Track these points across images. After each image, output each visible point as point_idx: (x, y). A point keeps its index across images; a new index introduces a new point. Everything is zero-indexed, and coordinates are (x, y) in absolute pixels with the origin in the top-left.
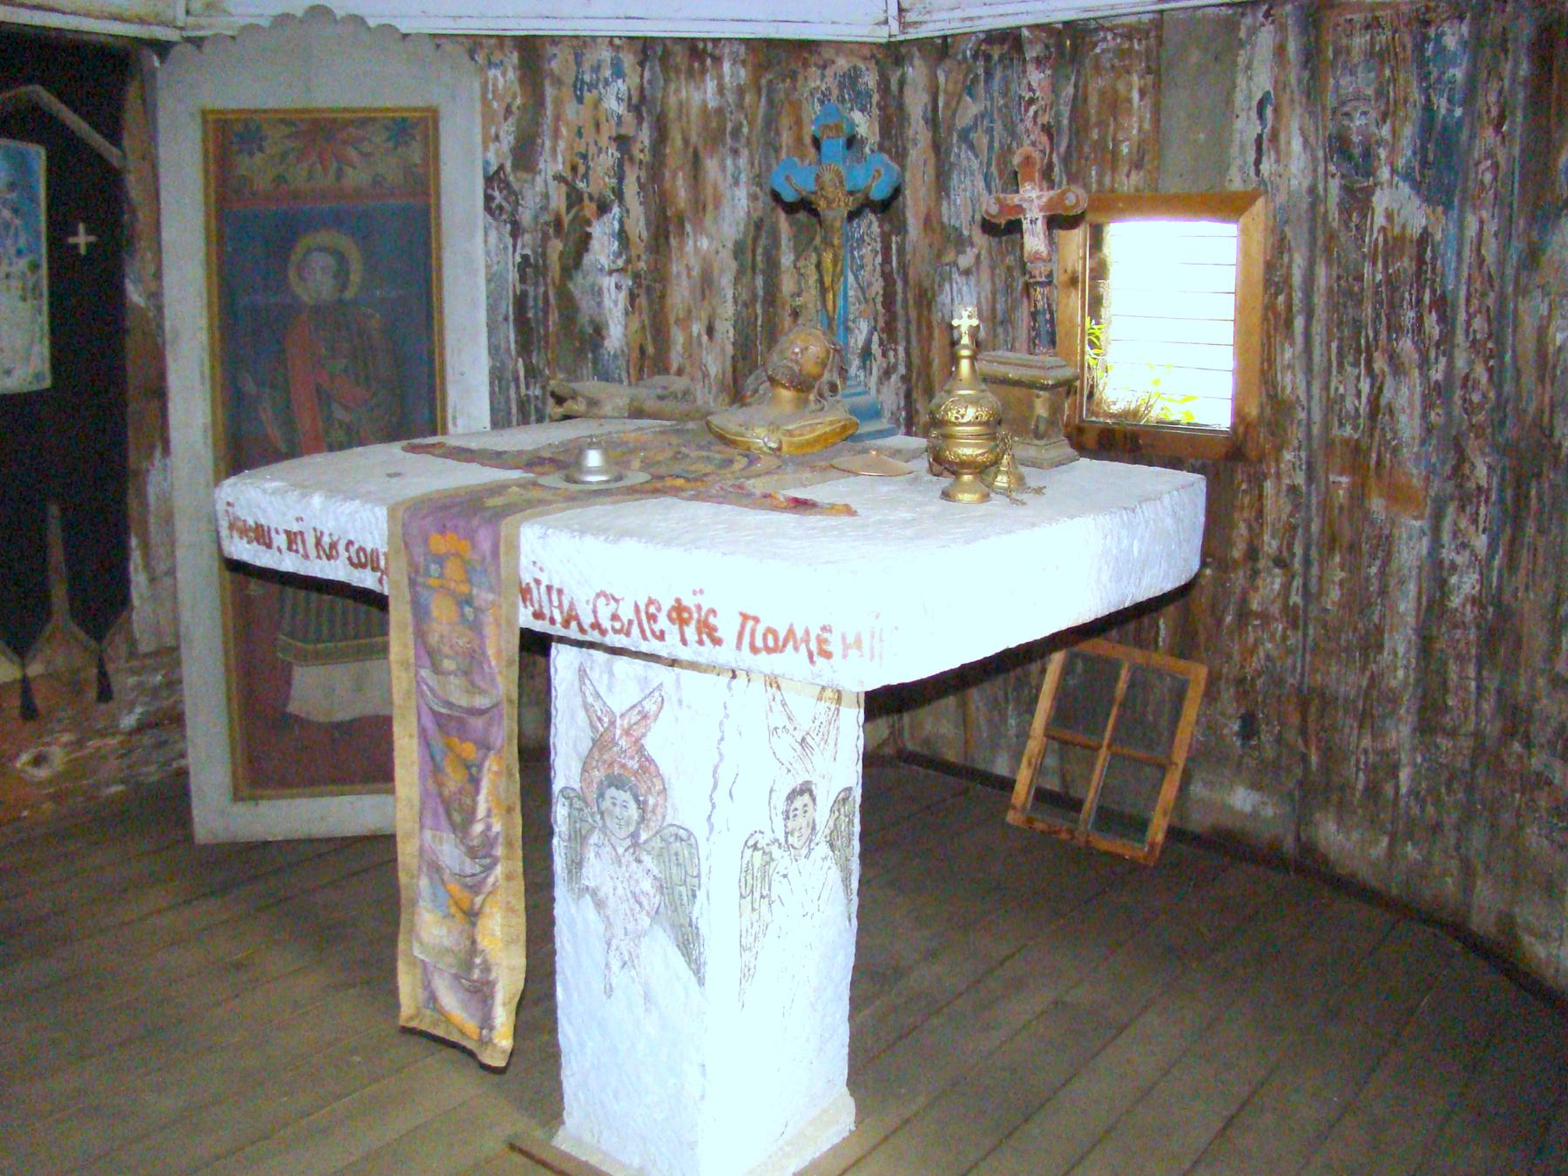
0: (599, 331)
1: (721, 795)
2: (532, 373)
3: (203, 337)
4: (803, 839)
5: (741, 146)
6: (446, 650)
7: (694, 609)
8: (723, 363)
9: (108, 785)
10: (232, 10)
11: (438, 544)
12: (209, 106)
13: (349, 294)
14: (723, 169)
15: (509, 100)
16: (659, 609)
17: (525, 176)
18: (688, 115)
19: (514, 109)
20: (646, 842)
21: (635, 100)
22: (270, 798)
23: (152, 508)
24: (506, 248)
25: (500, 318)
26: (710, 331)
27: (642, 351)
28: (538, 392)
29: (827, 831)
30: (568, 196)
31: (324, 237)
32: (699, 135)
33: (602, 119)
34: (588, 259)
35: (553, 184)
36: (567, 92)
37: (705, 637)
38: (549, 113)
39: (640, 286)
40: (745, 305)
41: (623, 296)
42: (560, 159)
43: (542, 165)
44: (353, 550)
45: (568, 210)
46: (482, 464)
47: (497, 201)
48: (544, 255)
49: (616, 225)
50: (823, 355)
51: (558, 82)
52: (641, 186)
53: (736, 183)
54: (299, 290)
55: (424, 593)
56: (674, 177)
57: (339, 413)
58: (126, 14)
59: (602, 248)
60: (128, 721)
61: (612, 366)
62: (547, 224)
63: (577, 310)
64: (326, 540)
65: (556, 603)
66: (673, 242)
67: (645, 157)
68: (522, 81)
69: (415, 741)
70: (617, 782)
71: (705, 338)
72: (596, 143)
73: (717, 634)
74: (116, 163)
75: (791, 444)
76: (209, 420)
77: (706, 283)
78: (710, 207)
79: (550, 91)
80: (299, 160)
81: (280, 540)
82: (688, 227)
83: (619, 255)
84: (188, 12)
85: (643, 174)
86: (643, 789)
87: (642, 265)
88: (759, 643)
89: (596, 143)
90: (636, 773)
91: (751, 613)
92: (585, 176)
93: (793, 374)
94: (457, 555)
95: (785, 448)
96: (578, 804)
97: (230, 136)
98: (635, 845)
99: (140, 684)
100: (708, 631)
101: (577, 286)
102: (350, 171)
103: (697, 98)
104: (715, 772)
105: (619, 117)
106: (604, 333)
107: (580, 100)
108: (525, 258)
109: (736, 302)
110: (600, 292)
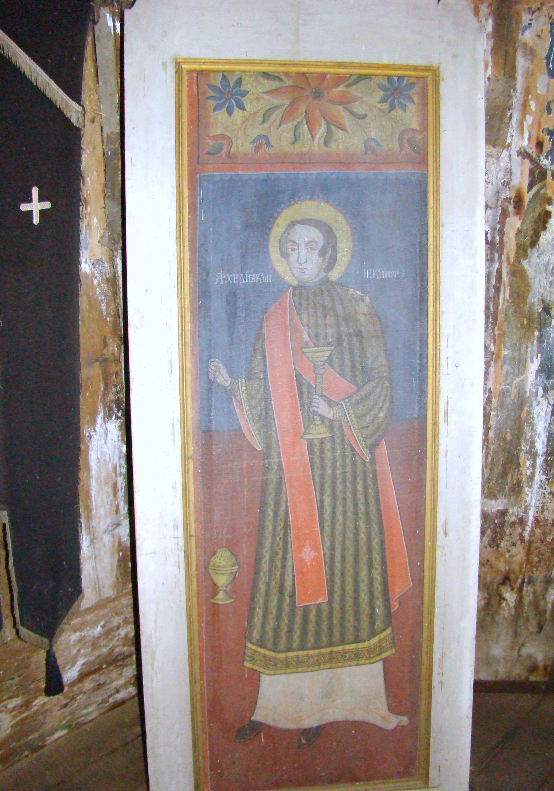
9: (52, 734)
12: (184, 54)
13: (335, 275)
23: (94, 473)
30: (531, 172)
31: (308, 208)
35: (517, 159)
38: (519, 86)
42: (526, 136)
45: (531, 186)
63: (528, 288)
74: (74, 119)
97: (205, 91)
102: (339, 134)
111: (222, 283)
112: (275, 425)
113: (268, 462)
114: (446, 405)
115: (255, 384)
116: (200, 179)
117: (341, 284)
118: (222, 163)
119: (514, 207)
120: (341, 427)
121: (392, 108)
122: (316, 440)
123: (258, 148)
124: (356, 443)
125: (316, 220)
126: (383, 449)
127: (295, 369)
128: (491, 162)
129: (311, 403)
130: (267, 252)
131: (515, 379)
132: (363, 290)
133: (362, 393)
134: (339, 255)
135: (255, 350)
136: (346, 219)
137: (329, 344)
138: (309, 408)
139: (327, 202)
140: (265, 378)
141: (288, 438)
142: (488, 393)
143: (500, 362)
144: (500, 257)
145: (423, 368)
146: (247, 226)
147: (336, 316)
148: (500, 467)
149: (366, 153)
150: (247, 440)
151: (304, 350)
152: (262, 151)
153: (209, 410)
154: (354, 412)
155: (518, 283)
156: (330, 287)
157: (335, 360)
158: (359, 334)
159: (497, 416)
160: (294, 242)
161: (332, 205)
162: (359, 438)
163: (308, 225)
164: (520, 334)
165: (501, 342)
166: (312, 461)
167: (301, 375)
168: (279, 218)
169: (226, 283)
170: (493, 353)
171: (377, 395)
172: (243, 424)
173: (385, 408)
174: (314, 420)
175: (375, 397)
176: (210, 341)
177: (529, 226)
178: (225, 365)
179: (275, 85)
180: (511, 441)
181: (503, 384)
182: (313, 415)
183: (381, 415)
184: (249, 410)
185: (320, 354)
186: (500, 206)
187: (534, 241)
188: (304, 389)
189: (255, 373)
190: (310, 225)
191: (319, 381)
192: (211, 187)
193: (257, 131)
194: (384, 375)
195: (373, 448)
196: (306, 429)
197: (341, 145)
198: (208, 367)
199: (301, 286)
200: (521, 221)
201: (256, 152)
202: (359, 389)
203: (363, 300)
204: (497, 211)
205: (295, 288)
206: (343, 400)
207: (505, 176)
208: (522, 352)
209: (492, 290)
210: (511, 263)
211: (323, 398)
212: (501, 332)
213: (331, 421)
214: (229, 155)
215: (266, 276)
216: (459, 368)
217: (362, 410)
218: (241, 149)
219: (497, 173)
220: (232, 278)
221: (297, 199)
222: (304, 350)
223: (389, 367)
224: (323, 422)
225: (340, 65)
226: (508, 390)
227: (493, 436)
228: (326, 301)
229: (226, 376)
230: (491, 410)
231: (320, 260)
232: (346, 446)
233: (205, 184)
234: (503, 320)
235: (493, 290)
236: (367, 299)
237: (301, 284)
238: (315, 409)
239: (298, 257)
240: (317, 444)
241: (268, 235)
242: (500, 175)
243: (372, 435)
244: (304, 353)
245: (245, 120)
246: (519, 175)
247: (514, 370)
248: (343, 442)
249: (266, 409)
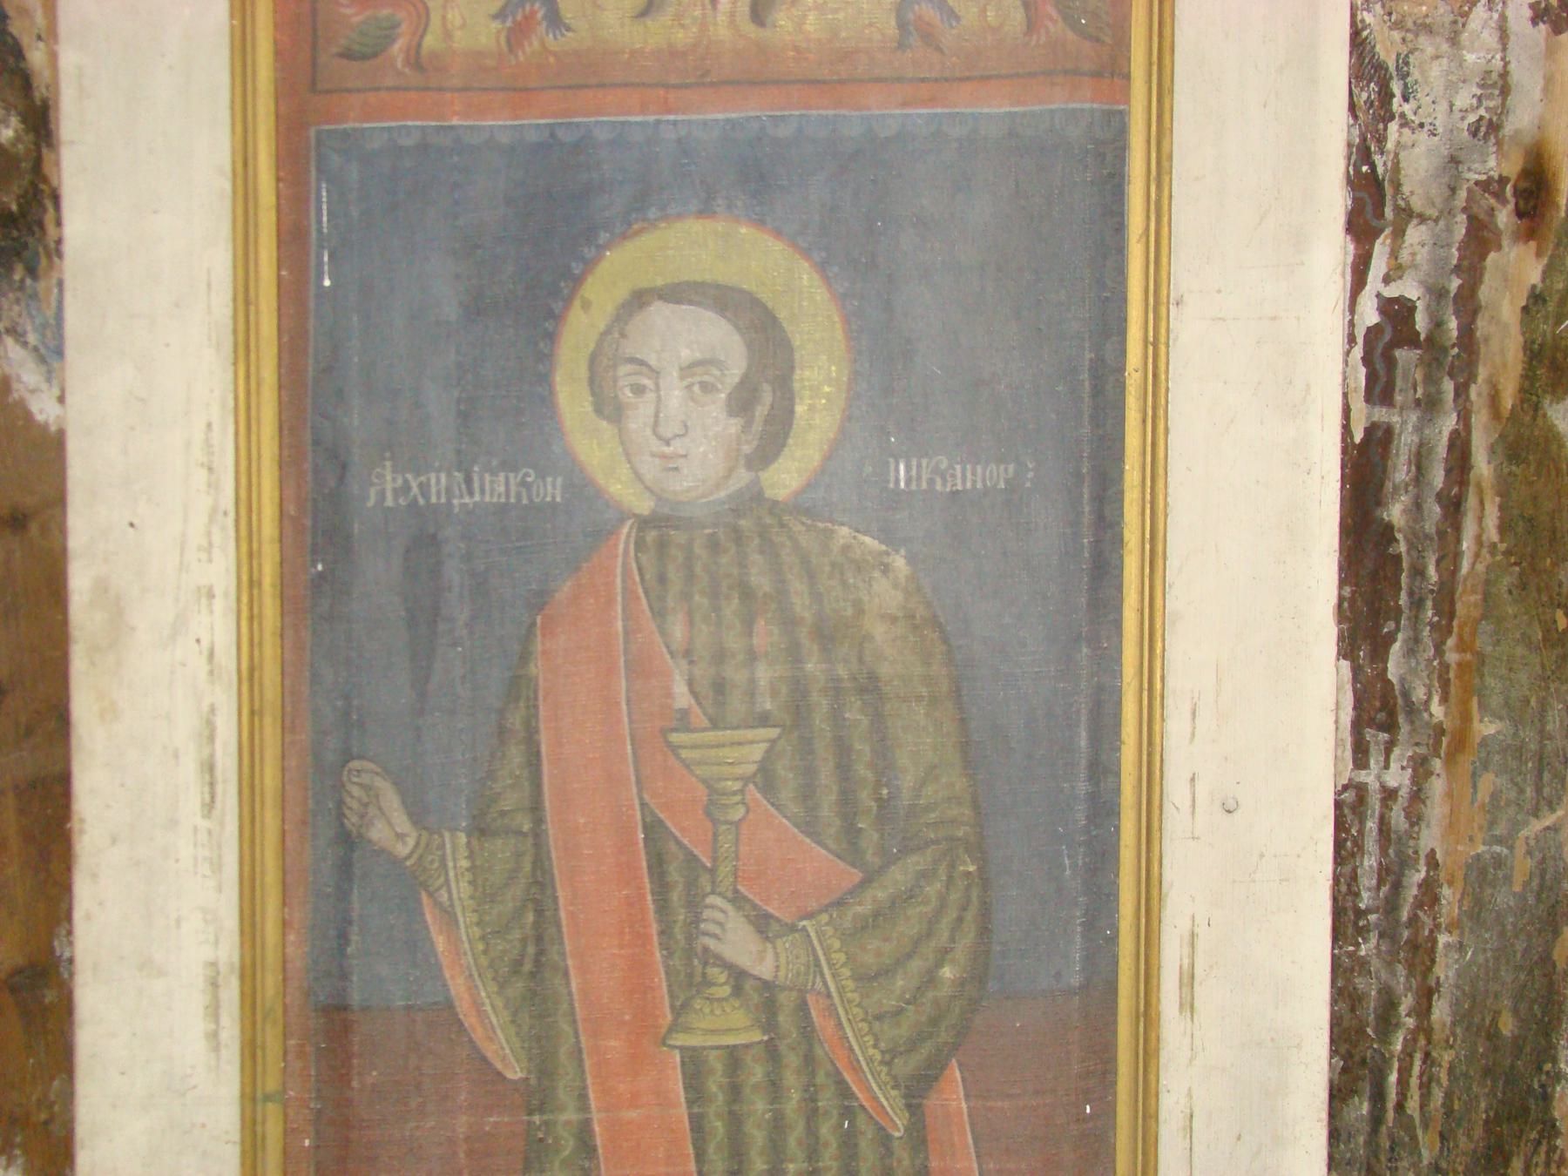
3: (217, 627)
13: (785, 478)
28: (1398, 777)
31: (692, 245)
48: (1468, 304)
76: (228, 951)
108: (1397, 312)
111: (389, 502)
112: (570, 994)
113: (546, 1123)
114: (1186, 950)
115: (501, 850)
116: (319, 142)
117: (808, 512)
118: (397, 89)
119: (1520, 214)
120: (802, 1008)
122: (714, 1053)
123: (517, 34)
124: (856, 1069)
125: (718, 287)
126: (952, 1096)
127: (643, 805)
128: (1430, 51)
129: (697, 920)
130: (547, 401)
131: (1526, 823)
132: (888, 535)
133: (879, 894)
134: (800, 409)
135: (502, 733)
136: (827, 280)
137: (764, 720)
138: (690, 939)
139: (759, 222)
140: (538, 835)
141: (613, 1043)
142: (1423, 870)
143: (1466, 762)
144: (1461, 391)
145: (1104, 809)
146: (476, 309)
147: (789, 622)
148: (1478, 1132)
149: (901, 46)
150: (471, 1041)
151: (675, 738)
152: (533, 45)
153: (343, 937)
154: (850, 958)
155: (1531, 484)
156: (768, 520)
157: (784, 770)
158: (870, 687)
159: (1461, 947)
160: (642, 363)
161: (778, 234)
162: (866, 1052)
163: (691, 303)
164: (1543, 666)
165: (1468, 691)
166: (698, 1125)
167: (661, 822)
168: (590, 280)
169: (402, 501)
170: (1440, 731)
171: (934, 903)
172: (458, 987)
173: (961, 951)
174: (707, 983)
175: (924, 909)
176: (347, 698)
178: (397, 784)
180: (1518, 1043)
181: (1479, 837)
182: (706, 964)
183: (947, 972)
184: (483, 938)
185: (730, 754)
186: (1464, 210)
188: (675, 875)
189: (503, 814)
190: (698, 304)
191: (726, 845)
192: (354, 173)
194: (960, 834)
195: (917, 1090)
196: (680, 1010)
197: (811, 17)
198: (339, 787)
199: (668, 518)
200: (1545, 260)
201: (511, 50)
202: (866, 882)
203: (886, 569)
204: (1449, 230)
205: (644, 523)
206: (810, 916)
207: (1480, 99)
208: (1549, 727)
209: (1434, 510)
210: (1506, 414)
211: (739, 908)
212: (1468, 656)
213: (767, 986)
214: (415, 60)
215: (543, 478)
216: (1237, 816)
217: (878, 954)
218: (461, 41)
219: (1451, 87)
220: (424, 488)
221: (652, 213)
222: (675, 738)
223: (975, 805)
224: (738, 991)
226: (1498, 862)
227: (1448, 1020)
228: (754, 571)
229: (402, 822)
230: (1437, 926)
231: (734, 425)
232: (820, 1078)
233: (335, 160)
234: (1476, 613)
235: (1437, 509)
236: (899, 562)
237: (666, 510)
238: (711, 943)
239: (657, 415)
240: (716, 1063)
241: (552, 337)
242: (1464, 99)
243: (912, 1045)
244: (674, 749)
246: (1537, 94)
247: (1521, 791)
248: (809, 1060)
249: (539, 939)
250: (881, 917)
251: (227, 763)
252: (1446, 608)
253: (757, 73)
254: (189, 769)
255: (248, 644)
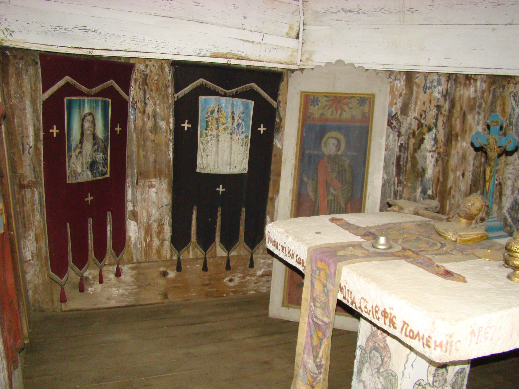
0: (424, 171)
1: (409, 365)
2: (400, 182)
3: (293, 162)
4: (440, 384)
5: (481, 111)
6: (317, 300)
7: (389, 314)
8: (467, 187)
10: (315, 61)
11: (320, 265)
13: (339, 153)
14: (474, 118)
15: (401, 91)
16: (379, 310)
17: (403, 117)
18: (463, 99)
19: (402, 94)
20: (382, 372)
21: (444, 93)
22: (293, 308)
24: (395, 140)
25: (391, 163)
26: (463, 175)
27: (438, 180)
28: (401, 189)
29: (452, 382)
30: (418, 124)
32: (466, 107)
33: (432, 99)
34: (422, 146)
35: (413, 120)
36: (421, 90)
37: (391, 325)
39: (440, 157)
40: (477, 167)
41: (434, 159)
42: (416, 112)
43: (410, 114)
44: (298, 257)
45: (418, 129)
46: (350, 232)
47: (394, 125)
48: (408, 144)
49: (434, 136)
50: (480, 207)
51: (418, 86)
52: (444, 123)
53: (478, 124)
54: (324, 149)
55: (314, 280)
56: (456, 121)
57: (332, 190)
58: (282, 61)
59: (428, 143)
60: (260, 273)
61: (427, 183)
62: (410, 133)
64: (291, 252)
65: (350, 296)
66: (453, 143)
67: (446, 113)
68: (406, 85)
69: (306, 325)
70: (376, 349)
71: (461, 177)
72: (429, 107)
73: (395, 325)
75: (461, 240)
76: (292, 188)
77: (464, 158)
78: (468, 132)
79: (415, 89)
80: (329, 109)
81: (280, 248)
82: (459, 138)
83: (433, 146)
84: (301, 61)
85: (445, 119)
86: (384, 354)
87: (441, 150)
88: (408, 334)
89: (429, 107)
90: (382, 348)
91: (407, 322)
92: (425, 118)
93: (466, 214)
94: (325, 270)
95: (458, 241)
96: (364, 352)
97: (309, 100)
98: (378, 372)
99: (264, 262)
100: (392, 323)
101: (418, 155)
102: (344, 113)
103: (467, 93)
104: (408, 356)
105: (438, 99)
106: (426, 172)
107: (425, 92)
108: (401, 144)
109: (473, 166)
110: (426, 158)
121: (360, 106)
172: (309, 192)
177: (418, 142)
179: (327, 99)
187: (419, 147)
193: (321, 112)
209: (405, 163)
213: (335, 195)
214: (313, 118)
225: (346, 94)
245: (318, 109)
250: (344, 190)
251: (293, 173)
252: (406, 173)
253: (340, 121)
254: (290, 173)
255: (296, 163)
